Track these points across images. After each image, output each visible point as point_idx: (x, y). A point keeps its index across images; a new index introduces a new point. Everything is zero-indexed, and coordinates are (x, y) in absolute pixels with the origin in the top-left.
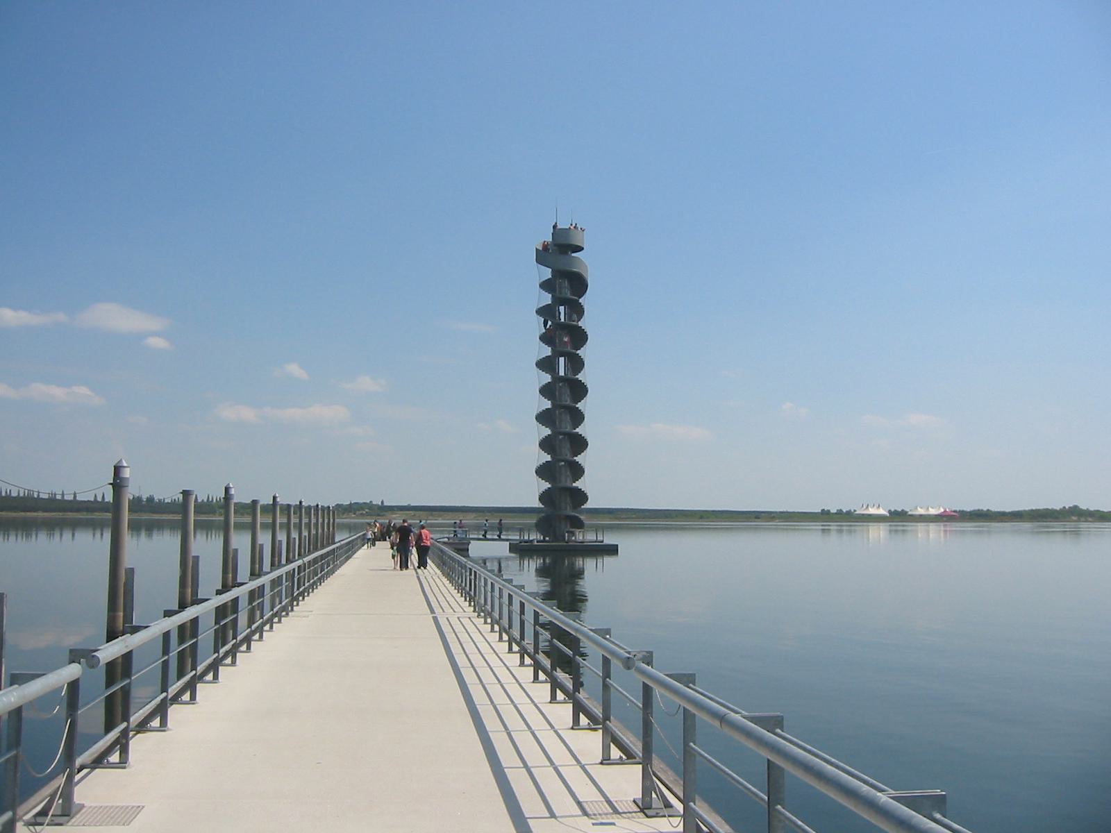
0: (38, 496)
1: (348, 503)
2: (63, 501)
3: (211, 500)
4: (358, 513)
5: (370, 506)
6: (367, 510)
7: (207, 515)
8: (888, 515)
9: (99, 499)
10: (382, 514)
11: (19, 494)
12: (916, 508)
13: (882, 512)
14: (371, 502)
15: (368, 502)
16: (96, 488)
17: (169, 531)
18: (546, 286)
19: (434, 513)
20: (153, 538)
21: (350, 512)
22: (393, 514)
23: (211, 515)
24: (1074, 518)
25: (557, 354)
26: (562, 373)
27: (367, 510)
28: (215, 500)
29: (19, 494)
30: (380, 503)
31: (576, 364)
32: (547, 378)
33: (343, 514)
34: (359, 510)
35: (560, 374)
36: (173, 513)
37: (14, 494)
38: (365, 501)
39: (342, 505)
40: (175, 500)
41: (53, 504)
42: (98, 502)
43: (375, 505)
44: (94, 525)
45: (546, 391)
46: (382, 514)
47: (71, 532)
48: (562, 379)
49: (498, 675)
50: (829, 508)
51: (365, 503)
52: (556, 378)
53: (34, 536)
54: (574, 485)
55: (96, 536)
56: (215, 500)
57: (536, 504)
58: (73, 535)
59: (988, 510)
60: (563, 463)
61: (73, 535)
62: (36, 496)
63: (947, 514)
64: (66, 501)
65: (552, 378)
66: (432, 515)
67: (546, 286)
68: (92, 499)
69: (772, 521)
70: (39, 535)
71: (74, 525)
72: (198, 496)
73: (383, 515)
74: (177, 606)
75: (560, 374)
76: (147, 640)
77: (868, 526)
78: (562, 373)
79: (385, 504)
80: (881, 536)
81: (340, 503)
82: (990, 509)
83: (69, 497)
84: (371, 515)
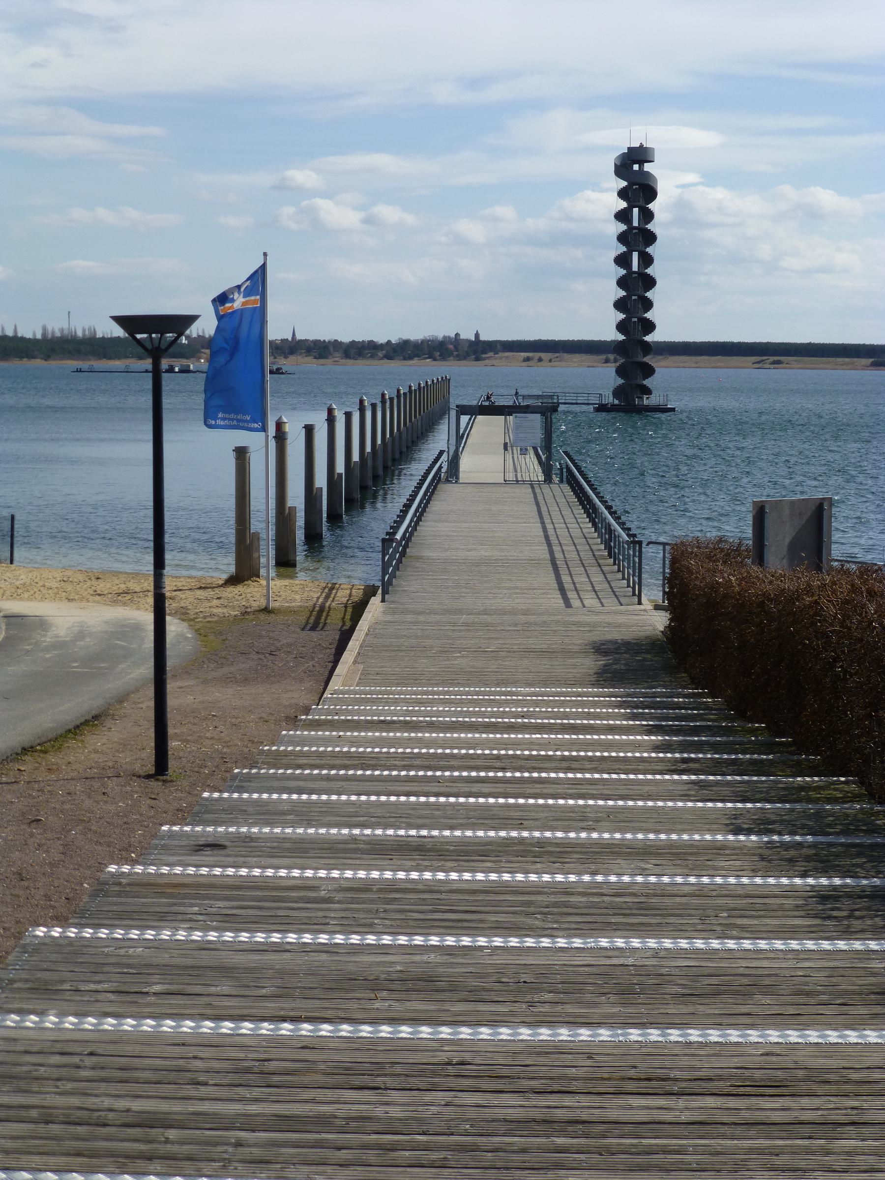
26: (635, 223)
48: (635, 228)
78: (635, 223)
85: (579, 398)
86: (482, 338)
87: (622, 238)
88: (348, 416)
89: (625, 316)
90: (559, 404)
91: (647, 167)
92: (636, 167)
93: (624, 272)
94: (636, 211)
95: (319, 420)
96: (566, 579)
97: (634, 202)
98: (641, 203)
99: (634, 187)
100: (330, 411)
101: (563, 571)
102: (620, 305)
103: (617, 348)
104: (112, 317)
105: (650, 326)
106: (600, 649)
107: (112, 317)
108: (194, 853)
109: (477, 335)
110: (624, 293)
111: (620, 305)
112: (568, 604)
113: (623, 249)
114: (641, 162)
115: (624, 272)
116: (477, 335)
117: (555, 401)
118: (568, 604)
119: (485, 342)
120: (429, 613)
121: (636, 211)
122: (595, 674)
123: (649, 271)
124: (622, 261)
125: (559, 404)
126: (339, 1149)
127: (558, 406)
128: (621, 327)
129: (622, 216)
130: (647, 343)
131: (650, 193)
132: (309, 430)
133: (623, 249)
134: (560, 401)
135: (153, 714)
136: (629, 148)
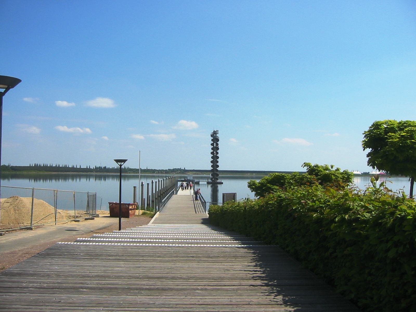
0: (69, 166)
1: (173, 169)
2: (76, 168)
3: (125, 167)
4: (176, 172)
5: (180, 170)
6: (179, 171)
7: (125, 173)
8: (361, 174)
9: (88, 168)
10: (184, 173)
11: (62, 166)
12: (372, 171)
13: (359, 173)
14: (181, 168)
15: (180, 168)
17: (71, 180)
19: (203, 172)
20: (110, 180)
21: (174, 172)
22: (188, 173)
23: (126, 173)
24: (273, 280)
26: (215, 146)
27: (179, 171)
28: (127, 168)
29: (62, 166)
30: (184, 169)
33: (171, 173)
34: (176, 171)
36: (55, 172)
37: (61, 166)
38: (178, 168)
39: (170, 169)
40: (113, 168)
41: (73, 169)
42: (88, 168)
43: (182, 169)
44: (113, 177)
46: (184, 173)
47: (29, 180)
50: (363, 172)
51: (178, 169)
53: (67, 180)
55: (87, 181)
56: (127, 168)
58: (80, 180)
59: (366, 172)
61: (80, 180)
62: (68, 167)
63: (382, 174)
64: (78, 168)
66: (202, 173)
70: (69, 181)
71: (80, 177)
72: (69, 165)
73: (185, 173)
74: (133, 202)
76: (384, 177)
77: (354, 178)
78: (215, 146)
80: (359, 181)
81: (170, 169)
82: (366, 172)
83: (78, 167)
84: (181, 173)
86: (186, 169)
87: (212, 149)
88: (161, 181)
91: (217, 135)
92: (215, 135)
93: (213, 147)
94: (215, 143)
95: (157, 181)
96: (196, 210)
98: (216, 150)
100: (159, 180)
101: (196, 208)
102: (212, 162)
103: (212, 171)
104: (127, 160)
105: (218, 166)
106: (203, 219)
107: (127, 160)
108: (49, 274)
109: (185, 168)
110: (212, 160)
111: (212, 162)
112: (196, 213)
113: (213, 142)
114: (216, 134)
115: (213, 147)
118: (196, 213)
119: (186, 170)
121: (215, 143)
123: (218, 155)
124: (212, 144)
128: (212, 166)
130: (217, 170)
131: (218, 140)
132: (156, 182)
133: (213, 142)
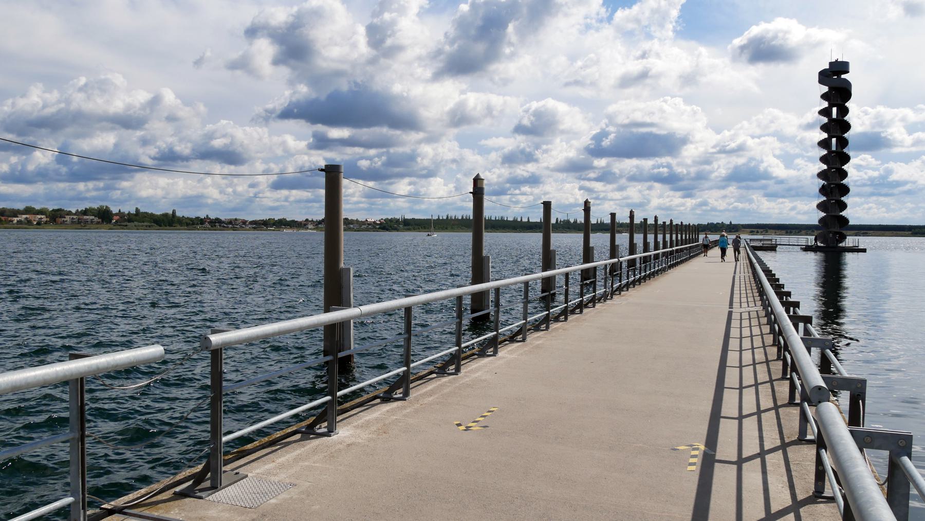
16: (537, 216)
18: (824, 97)
25: (831, 106)
26: (834, 148)
31: (844, 111)
32: (825, 152)
35: (833, 117)
37: (493, 218)
45: (823, 159)
48: (833, 152)
49: (730, 420)
52: (830, 152)
54: (841, 214)
57: (817, 223)
60: (834, 201)
65: (828, 120)
67: (824, 97)
68: (539, 221)
69: (42, 363)
75: (833, 117)
78: (834, 148)
79: (849, 257)
83: (525, 220)
85: (790, 241)
89: (825, 214)
90: (777, 245)
97: (832, 181)
99: (833, 170)
104: (478, 174)
107: (478, 174)
109: (731, 222)
116: (731, 222)
117: (774, 243)
120: (5, 285)
121: (834, 140)
122: (890, 296)
125: (777, 245)
126: (869, 340)
127: (776, 247)
129: (825, 112)
134: (778, 243)
135: (848, 403)
136: (831, 64)
